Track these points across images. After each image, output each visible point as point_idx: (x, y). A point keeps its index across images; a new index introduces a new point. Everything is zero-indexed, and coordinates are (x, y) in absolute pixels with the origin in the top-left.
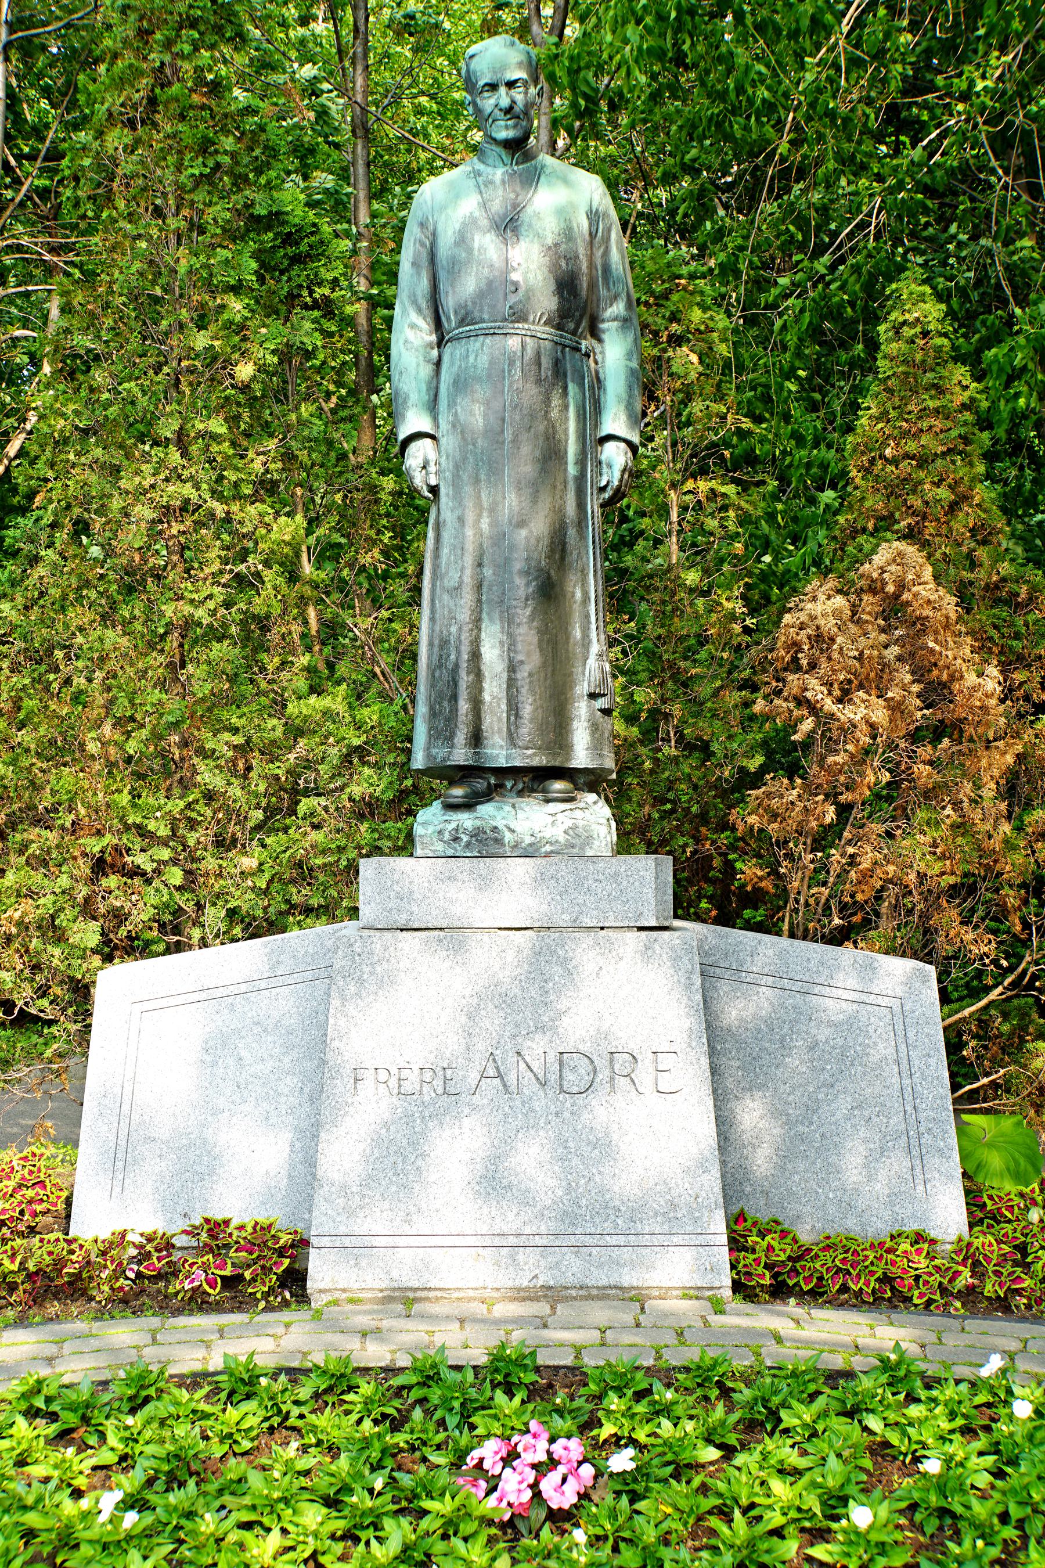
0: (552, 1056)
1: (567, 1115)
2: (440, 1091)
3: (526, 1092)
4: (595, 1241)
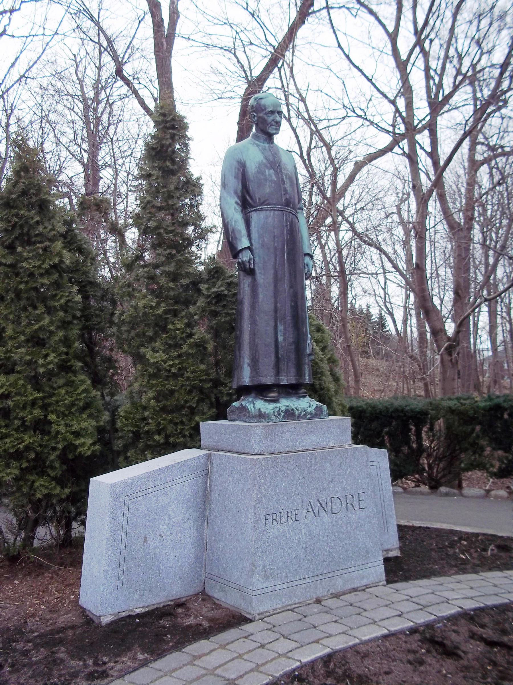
0: (329, 499)
1: (334, 522)
2: (294, 520)
3: (321, 515)
4: (346, 571)
